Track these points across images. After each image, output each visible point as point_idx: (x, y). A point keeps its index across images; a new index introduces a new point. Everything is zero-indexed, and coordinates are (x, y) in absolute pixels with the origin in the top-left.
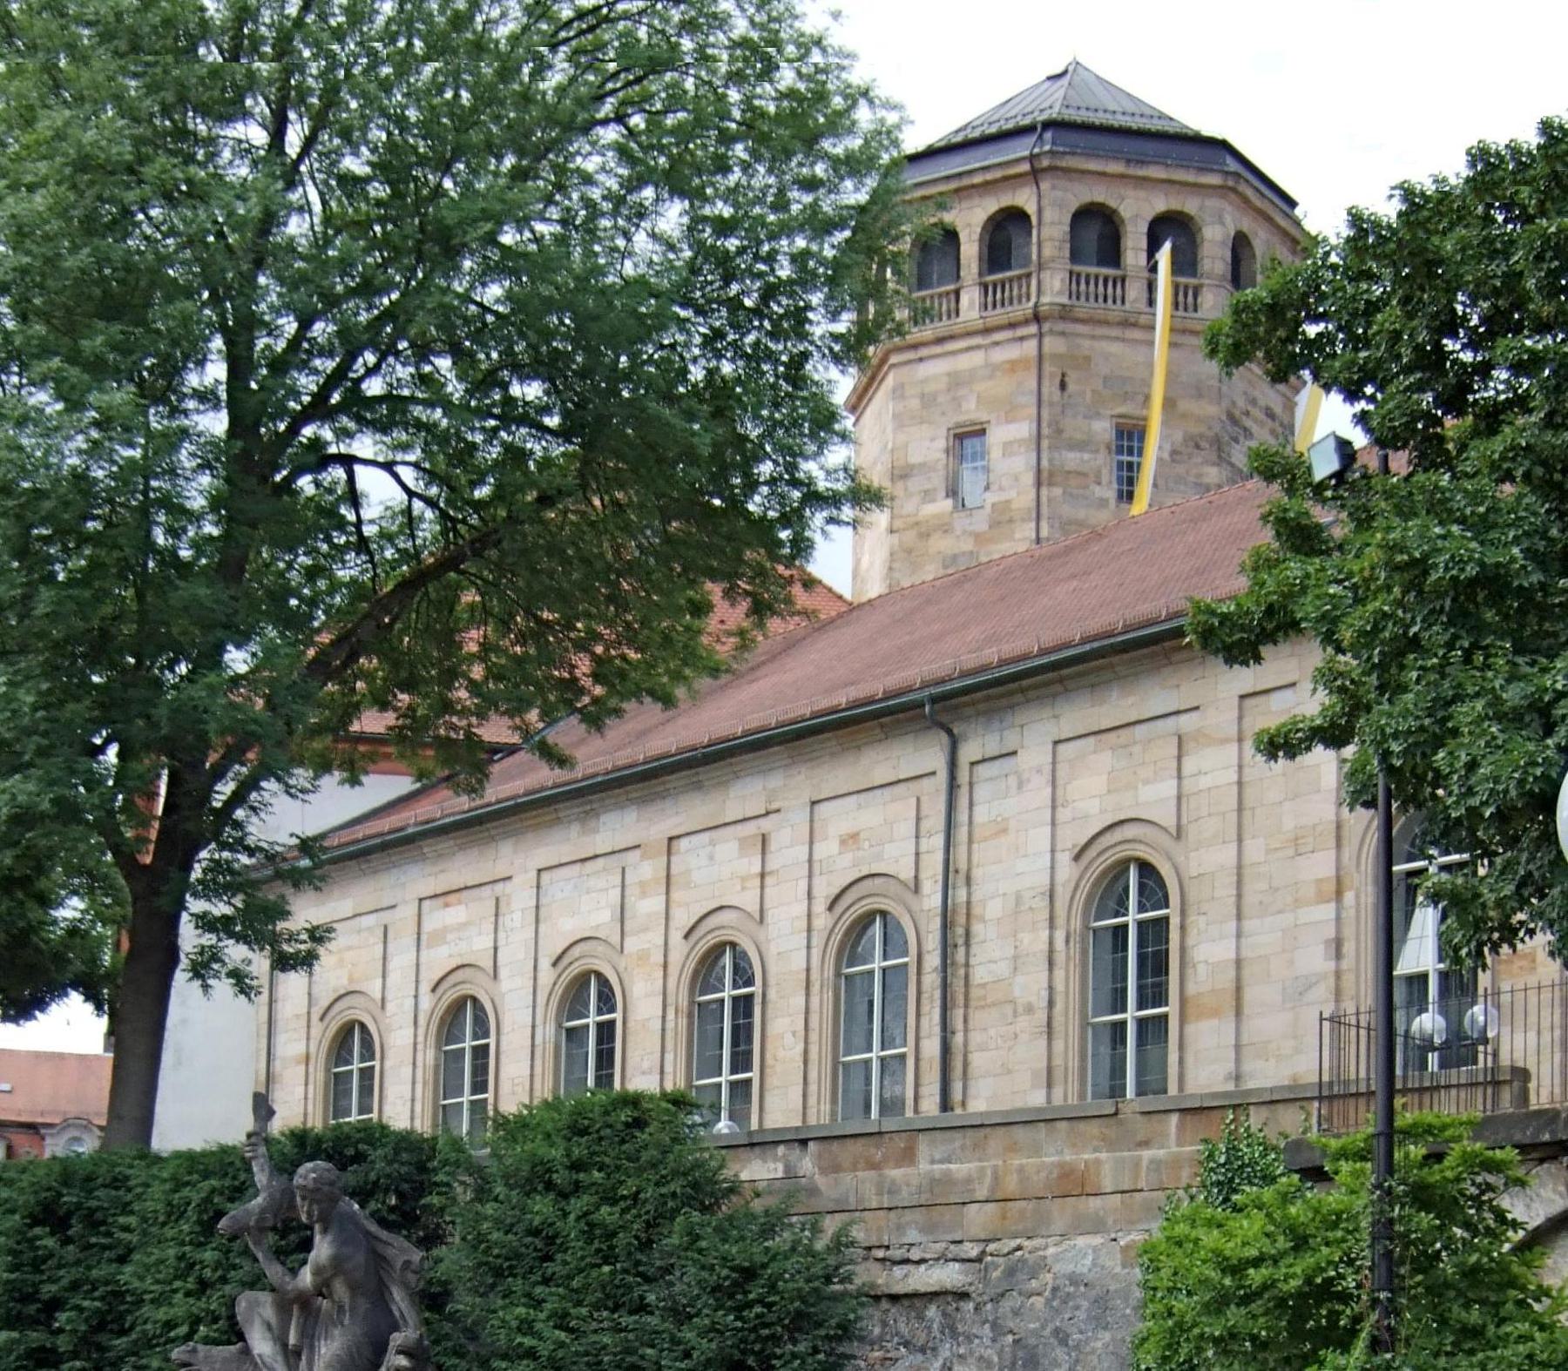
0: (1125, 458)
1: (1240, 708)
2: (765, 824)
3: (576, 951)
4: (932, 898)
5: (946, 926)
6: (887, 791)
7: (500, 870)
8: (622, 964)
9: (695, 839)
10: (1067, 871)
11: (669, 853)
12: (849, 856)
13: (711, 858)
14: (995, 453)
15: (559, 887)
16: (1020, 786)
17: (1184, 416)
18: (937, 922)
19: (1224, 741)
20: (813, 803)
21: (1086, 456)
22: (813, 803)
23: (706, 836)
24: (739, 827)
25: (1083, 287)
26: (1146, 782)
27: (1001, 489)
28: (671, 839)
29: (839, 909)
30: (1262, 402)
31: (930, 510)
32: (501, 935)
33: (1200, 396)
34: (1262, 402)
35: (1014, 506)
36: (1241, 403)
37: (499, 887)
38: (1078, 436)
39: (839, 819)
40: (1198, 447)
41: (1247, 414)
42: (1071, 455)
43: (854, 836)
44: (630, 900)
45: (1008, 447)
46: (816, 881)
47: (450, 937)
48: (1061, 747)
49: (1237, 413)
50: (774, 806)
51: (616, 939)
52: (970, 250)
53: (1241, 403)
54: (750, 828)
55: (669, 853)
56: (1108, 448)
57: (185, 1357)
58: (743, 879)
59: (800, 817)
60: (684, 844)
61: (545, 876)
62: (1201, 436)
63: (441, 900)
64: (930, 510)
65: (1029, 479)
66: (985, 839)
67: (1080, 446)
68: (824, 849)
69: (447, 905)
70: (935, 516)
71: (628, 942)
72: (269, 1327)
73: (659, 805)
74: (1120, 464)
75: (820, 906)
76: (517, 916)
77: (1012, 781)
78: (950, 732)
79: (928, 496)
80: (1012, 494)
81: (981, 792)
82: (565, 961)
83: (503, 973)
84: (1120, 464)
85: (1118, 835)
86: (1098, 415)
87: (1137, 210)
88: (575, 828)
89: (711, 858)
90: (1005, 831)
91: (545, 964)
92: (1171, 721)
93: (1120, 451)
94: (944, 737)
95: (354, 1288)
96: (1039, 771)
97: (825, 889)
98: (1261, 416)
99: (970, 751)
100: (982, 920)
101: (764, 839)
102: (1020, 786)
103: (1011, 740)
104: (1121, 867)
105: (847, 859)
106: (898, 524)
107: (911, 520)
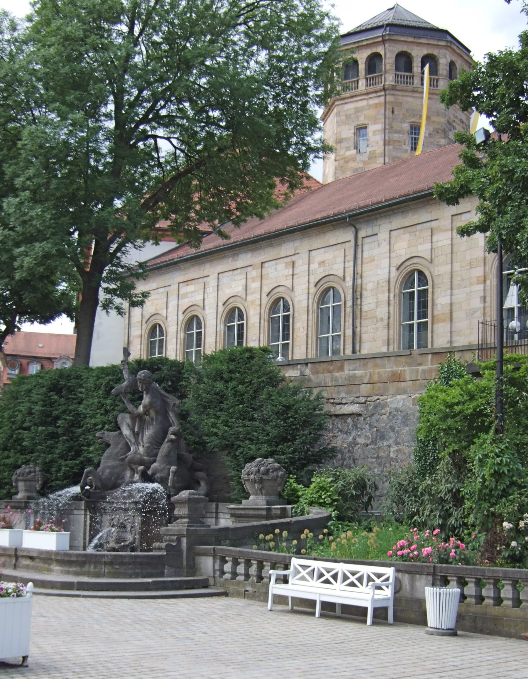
0: (414, 136)
2: (294, 258)
3: (231, 300)
6: (334, 247)
7: (206, 273)
10: (394, 273)
12: (322, 268)
13: (276, 269)
14: (370, 134)
15: (225, 279)
16: (379, 245)
17: (433, 122)
18: (351, 291)
20: (310, 251)
21: (401, 135)
22: (310, 251)
24: (285, 259)
25: (399, 79)
26: (420, 244)
28: (262, 263)
30: (459, 117)
32: (206, 295)
34: (459, 117)
36: (452, 118)
37: (205, 279)
38: (398, 129)
39: (318, 256)
41: (454, 121)
42: (396, 135)
43: (323, 262)
44: (249, 283)
45: (374, 133)
46: (311, 277)
47: (189, 295)
48: (392, 232)
49: (451, 121)
50: (297, 252)
51: (244, 296)
52: (362, 67)
53: (452, 118)
54: (289, 259)
56: (408, 132)
57: (100, 436)
58: (286, 276)
60: (266, 265)
61: (221, 275)
62: (439, 129)
63: (186, 283)
67: (398, 132)
69: (188, 285)
71: (248, 297)
72: (129, 425)
74: (412, 138)
75: (312, 285)
76: (211, 289)
77: (376, 243)
78: (355, 227)
79: (348, 149)
80: (376, 148)
81: (366, 247)
82: (227, 304)
83: (207, 307)
86: (404, 122)
87: (417, 53)
88: (230, 260)
90: (374, 260)
91: (220, 304)
92: (429, 224)
95: (157, 412)
97: (314, 280)
101: (293, 263)
102: (379, 245)
103: (375, 230)
104: (412, 272)
105: (321, 269)
106: (338, 158)
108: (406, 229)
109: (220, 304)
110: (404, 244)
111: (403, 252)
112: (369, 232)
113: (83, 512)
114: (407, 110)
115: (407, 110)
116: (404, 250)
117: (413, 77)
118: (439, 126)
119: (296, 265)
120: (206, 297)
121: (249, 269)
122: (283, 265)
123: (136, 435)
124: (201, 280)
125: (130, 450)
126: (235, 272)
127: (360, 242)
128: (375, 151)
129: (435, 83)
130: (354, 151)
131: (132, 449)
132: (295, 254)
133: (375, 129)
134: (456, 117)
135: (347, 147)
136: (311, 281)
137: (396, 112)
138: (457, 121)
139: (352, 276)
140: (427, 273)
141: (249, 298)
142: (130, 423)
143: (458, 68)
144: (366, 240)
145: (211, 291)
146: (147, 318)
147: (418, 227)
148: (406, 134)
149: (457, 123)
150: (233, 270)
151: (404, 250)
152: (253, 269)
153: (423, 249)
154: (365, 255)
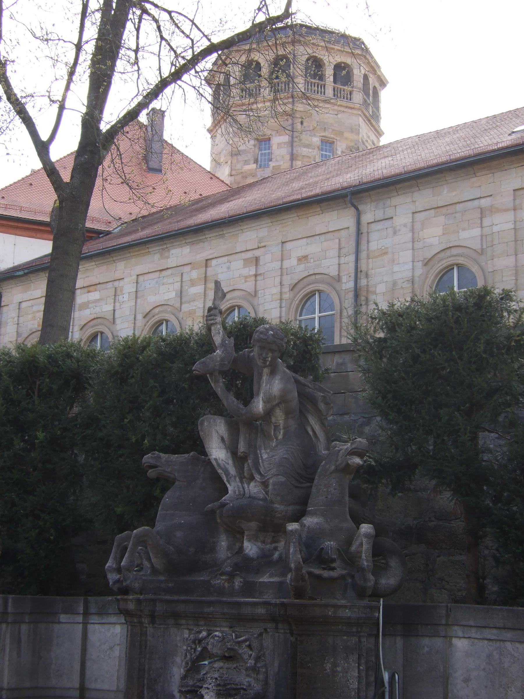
0: (324, 153)
1: (514, 195)
2: (257, 253)
3: (157, 310)
4: (348, 284)
5: (357, 296)
6: (322, 237)
7: (118, 275)
8: (181, 316)
9: (220, 260)
10: (419, 271)
11: (206, 266)
12: (303, 266)
13: (229, 268)
14: (274, 147)
15: (148, 283)
16: (395, 233)
17: (347, 139)
18: (351, 295)
19: (507, 210)
20: (283, 243)
21: (310, 150)
22: (283, 243)
23: (225, 259)
24: (243, 254)
25: (310, 87)
26: (464, 230)
27: (277, 161)
28: (207, 260)
29: (296, 289)
30: (371, 138)
31: (247, 168)
32: (117, 304)
33: (352, 132)
34: (371, 138)
35: (282, 167)
36: (365, 137)
37: (116, 284)
38: (307, 142)
39: (298, 249)
40: (351, 151)
41: (367, 141)
42: (305, 149)
43: (305, 257)
44: (186, 288)
45: (279, 145)
46: (284, 277)
47: (90, 305)
48: (416, 215)
49: (364, 140)
50: (262, 244)
51: (178, 305)
52: (265, 71)
53: (365, 137)
54: (249, 255)
55: (206, 266)
56: (318, 147)
57: (152, 461)
58: (246, 277)
59: (276, 250)
60: (214, 262)
61: (141, 279)
62: (353, 147)
63: (86, 290)
64: (247, 168)
65: (288, 157)
66: (376, 257)
67: (308, 146)
68: (291, 262)
69: (89, 292)
70: (249, 170)
71: (184, 306)
72: (223, 439)
73: (201, 245)
74: (322, 155)
75: (286, 289)
76: (126, 296)
77: (390, 231)
78: (357, 209)
79: (246, 162)
80: (282, 163)
81: (373, 236)
82: (150, 315)
83: (118, 321)
84: (322, 155)
85: (448, 253)
86: (315, 135)
87: (330, 61)
88: (157, 256)
89: (229, 268)
90: (386, 253)
91: (140, 317)
92: (476, 203)
93: (322, 150)
94: (353, 210)
95: (288, 413)
96: (405, 226)
97: (288, 281)
98: (371, 143)
99: (367, 218)
100: (375, 293)
101: (257, 259)
102: (395, 233)
103: (389, 212)
104: (449, 269)
105: (302, 267)
106: (234, 173)
107: (240, 171)
108: (438, 210)
109: (140, 317)
110: (438, 230)
111: (435, 241)
112: (379, 215)
113: (80, 619)
114: (317, 122)
115: (317, 122)
116: (437, 238)
117: (324, 86)
118: (352, 144)
119: (261, 262)
120: (117, 308)
121: (187, 269)
122: (241, 263)
123: (239, 460)
124: (110, 285)
125: (226, 491)
126: (164, 273)
127: (364, 229)
128: (280, 165)
129: (349, 96)
130: (254, 166)
131: (230, 489)
132: (259, 248)
133: (280, 141)
134: (369, 137)
135: (245, 161)
136: (284, 282)
137: (305, 124)
138: (369, 141)
139: (353, 275)
140: (475, 269)
141: (186, 308)
142: (226, 436)
143: (370, 83)
144: (374, 227)
145: (126, 299)
146: (26, 336)
147: (458, 207)
148: (317, 149)
149: (369, 144)
150: (161, 271)
151: (437, 238)
152: (193, 269)
153: (469, 236)
154: (373, 246)
